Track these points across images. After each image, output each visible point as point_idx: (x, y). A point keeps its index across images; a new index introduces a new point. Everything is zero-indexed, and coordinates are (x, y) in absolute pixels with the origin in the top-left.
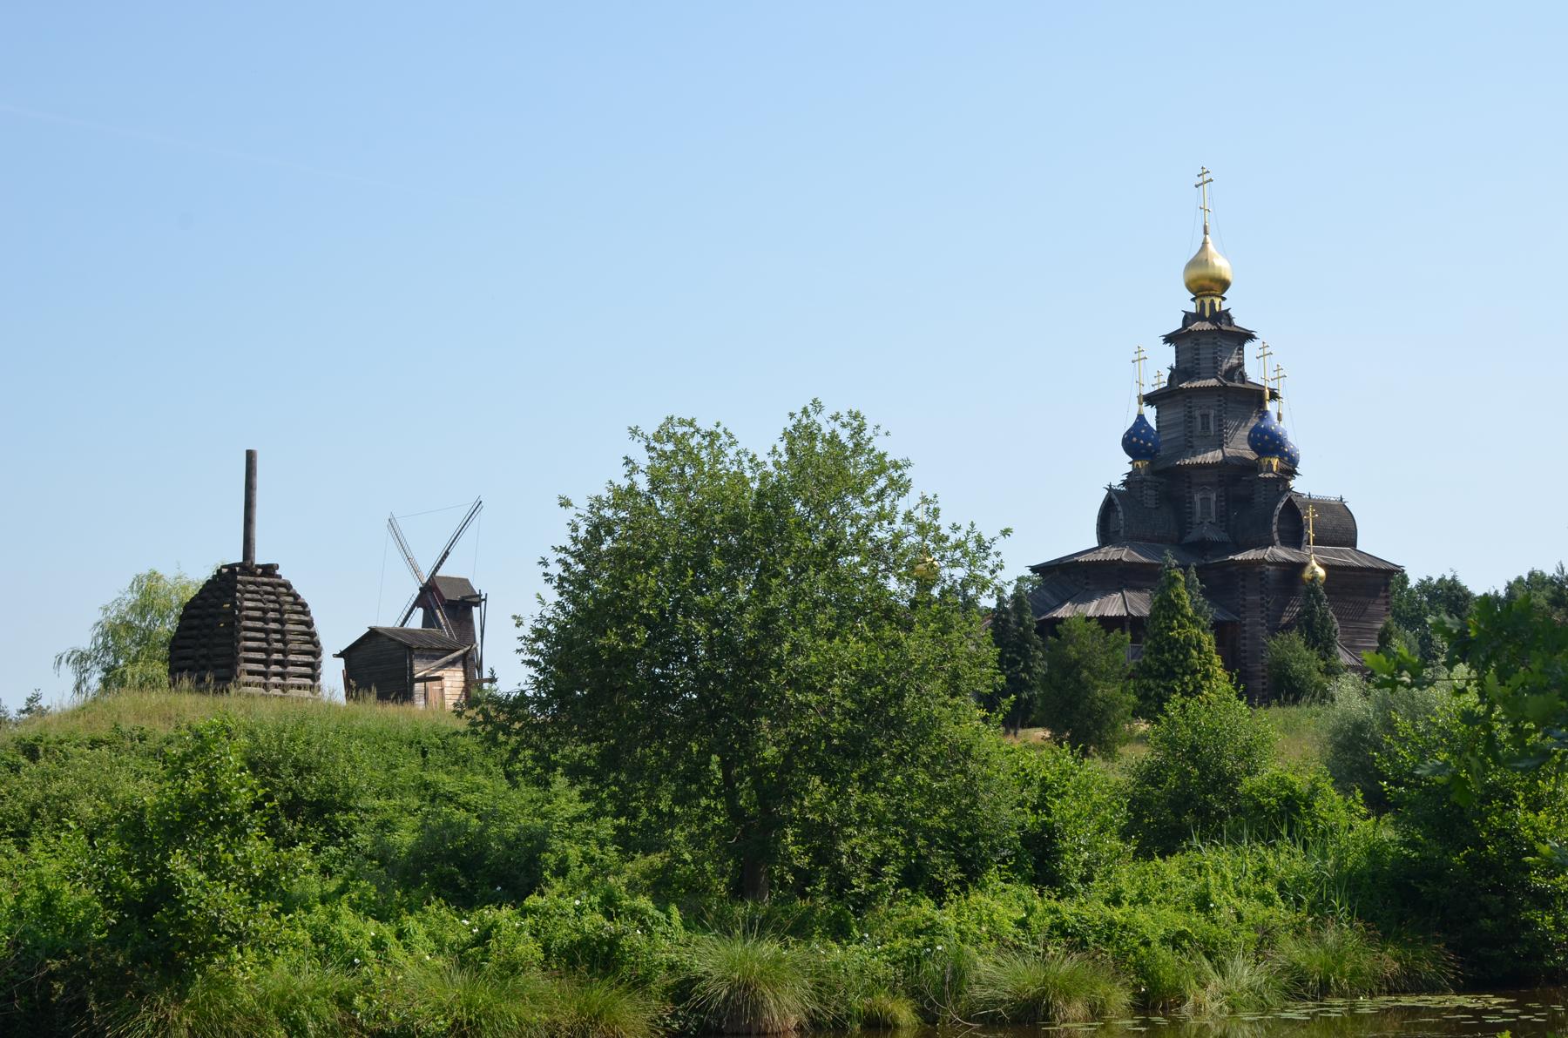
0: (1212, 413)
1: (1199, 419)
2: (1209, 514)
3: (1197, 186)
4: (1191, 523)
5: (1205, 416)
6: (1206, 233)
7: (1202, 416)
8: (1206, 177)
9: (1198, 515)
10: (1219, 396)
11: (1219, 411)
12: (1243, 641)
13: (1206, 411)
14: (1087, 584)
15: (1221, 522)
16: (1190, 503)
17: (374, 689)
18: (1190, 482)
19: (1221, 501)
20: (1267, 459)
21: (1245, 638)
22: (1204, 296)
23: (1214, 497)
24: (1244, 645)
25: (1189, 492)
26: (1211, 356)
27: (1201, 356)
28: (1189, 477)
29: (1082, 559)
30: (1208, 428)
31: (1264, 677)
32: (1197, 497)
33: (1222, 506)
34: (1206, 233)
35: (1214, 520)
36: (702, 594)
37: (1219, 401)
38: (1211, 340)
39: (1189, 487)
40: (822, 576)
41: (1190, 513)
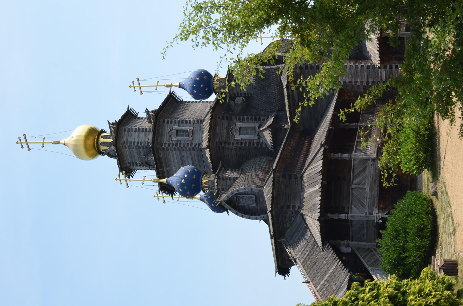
0: (176, 127)
1: (179, 138)
2: (252, 128)
3: (29, 149)
4: (258, 144)
5: (178, 133)
6: (58, 143)
7: (177, 136)
8: (23, 141)
9: (252, 137)
10: (164, 122)
11: (175, 123)
12: (359, 84)
13: (174, 132)
14: (294, 207)
15: (260, 119)
16: (242, 143)
17: (316, 73)
18: (225, 143)
19: (243, 119)
20: (215, 82)
21: (356, 82)
22: (97, 143)
23: (239, 124)
24: (362, 82)
25: (233, 144)
26: (137, 133)
27: (136, 141)
28: (221, 143)
29: (272, 233)
30: (187, 131)
31: (391, 67)
32: (238, 137)
33: (247, 118)
34: (58, 143)
35: (258, 125)
36: (370, 290)
37: (168, 122)
38: (126, 133)
39: (229, 144)
40: (418, 286)
41: (250, 143)
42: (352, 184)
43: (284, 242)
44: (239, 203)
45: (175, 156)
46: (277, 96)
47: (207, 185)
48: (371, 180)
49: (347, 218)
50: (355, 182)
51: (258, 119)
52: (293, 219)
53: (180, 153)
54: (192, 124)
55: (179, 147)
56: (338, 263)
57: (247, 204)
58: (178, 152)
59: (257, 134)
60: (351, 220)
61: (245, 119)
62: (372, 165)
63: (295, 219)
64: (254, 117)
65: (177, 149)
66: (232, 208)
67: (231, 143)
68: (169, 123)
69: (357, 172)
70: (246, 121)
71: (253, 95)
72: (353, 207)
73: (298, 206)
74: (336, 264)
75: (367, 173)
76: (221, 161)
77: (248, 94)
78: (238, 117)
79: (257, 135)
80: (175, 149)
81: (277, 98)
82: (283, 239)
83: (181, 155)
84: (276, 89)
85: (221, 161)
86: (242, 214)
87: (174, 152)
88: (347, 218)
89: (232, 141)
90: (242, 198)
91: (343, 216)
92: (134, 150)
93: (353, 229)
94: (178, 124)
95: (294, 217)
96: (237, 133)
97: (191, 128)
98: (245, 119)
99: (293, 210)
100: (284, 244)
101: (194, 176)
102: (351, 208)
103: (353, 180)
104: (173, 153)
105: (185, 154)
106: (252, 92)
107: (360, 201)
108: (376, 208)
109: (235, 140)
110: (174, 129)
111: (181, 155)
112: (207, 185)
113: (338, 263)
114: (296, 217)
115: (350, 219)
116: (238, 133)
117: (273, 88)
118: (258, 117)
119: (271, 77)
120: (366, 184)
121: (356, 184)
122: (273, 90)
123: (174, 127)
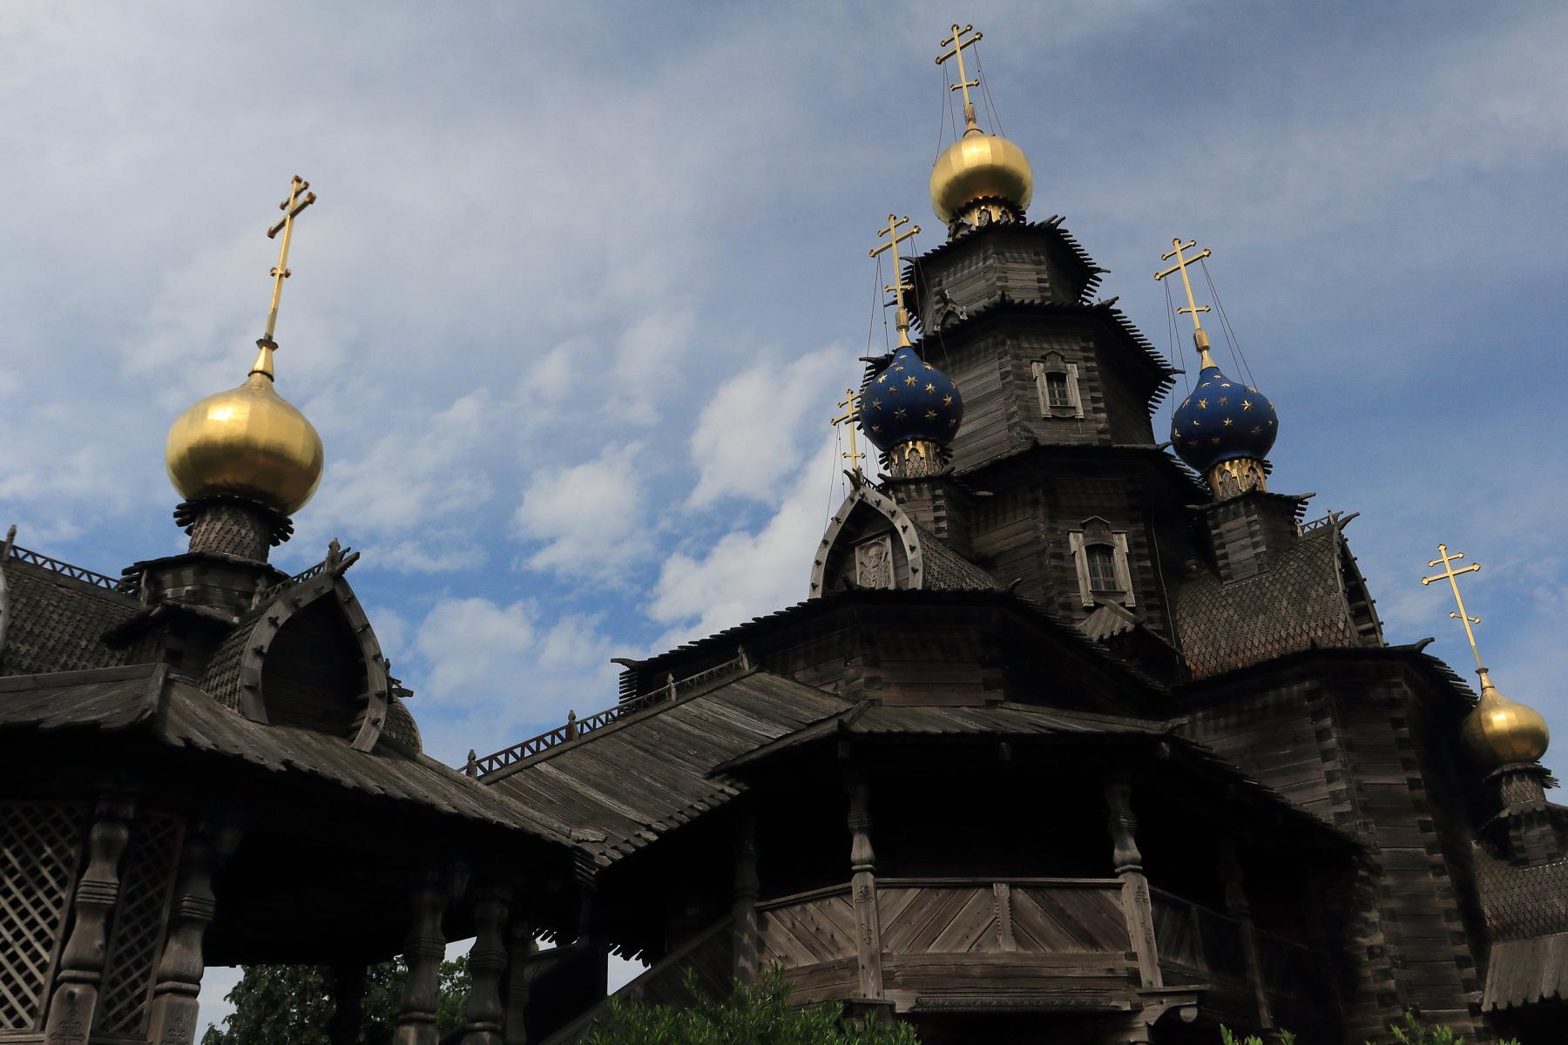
1: (1042, 384)
42: (1012, 886)
43: (737, 665)
44: (862, 548)
45: (985, 380)
46: (1241, 655)
47: (907, 458)
48: (1046, 972)
49: (854, 868)
50: (1021, 896)
51: (1149, 601)
52: (829, 689)
53: (998, 392)
54: (877, 1029)
55: (1016, 385)
56: (649, 828)
57: (862, 573)
58: (999, 385)
59: (1098, 601)
60: (848, 892)
61: (1142, 564)
62: (1111, 970)
63: (829, 694)
64: (1153, 588)
65: (1008, 380)
66: (841, 525)
67: (1054, 526)
68: (1085, 354)
69: (1070, 903)
70: (1136, 565)
71: (1225, 583)
72: (912, 894)
73: (881, 700)
74: (647, 820)
75: (1071, 950)
76: (991, 494)
77: (1227, 566)
78: (1144, 539)
79: (1095, 603)
80: (1004, 376)
81: (1234, 657)
82: (747, 666)
83: (989, 397)
84: (1269, 648)
85: (991, 494)
86: (824, 561)
87: (997, 375)
88: (854, 868)
89: (1061, 528)
90: (881, 553)
91: (861, 850)
92: (981, 284)
93: (811, 907)
94: (1086, 377)
95: (835, 689)
96: (1092, 539)
97: (1081, 414)
98: (1142, 564)
99: (862, 680)
100: (730, 665)
101: (932, 414)
102: (905, 887)
103: (1027, 887)
104: (991, 372)
105: (992, 406)
106: (1236, 578)
107: (940, 924)
108: (917, 1001)
109: (1068, 534)
110: (1069, 366)
111: (989, 397)
112: (907, 458)
113: (649, 828)
114: (837, 696)
115: (852, 883)
116: (1092, 541)
117: (1270, 639)
118: (1155, 601)
119: (1313, 624)
120: (1021, 951)
121: (1011, 900)
122: (1263, 640)
123: (1075, 365)
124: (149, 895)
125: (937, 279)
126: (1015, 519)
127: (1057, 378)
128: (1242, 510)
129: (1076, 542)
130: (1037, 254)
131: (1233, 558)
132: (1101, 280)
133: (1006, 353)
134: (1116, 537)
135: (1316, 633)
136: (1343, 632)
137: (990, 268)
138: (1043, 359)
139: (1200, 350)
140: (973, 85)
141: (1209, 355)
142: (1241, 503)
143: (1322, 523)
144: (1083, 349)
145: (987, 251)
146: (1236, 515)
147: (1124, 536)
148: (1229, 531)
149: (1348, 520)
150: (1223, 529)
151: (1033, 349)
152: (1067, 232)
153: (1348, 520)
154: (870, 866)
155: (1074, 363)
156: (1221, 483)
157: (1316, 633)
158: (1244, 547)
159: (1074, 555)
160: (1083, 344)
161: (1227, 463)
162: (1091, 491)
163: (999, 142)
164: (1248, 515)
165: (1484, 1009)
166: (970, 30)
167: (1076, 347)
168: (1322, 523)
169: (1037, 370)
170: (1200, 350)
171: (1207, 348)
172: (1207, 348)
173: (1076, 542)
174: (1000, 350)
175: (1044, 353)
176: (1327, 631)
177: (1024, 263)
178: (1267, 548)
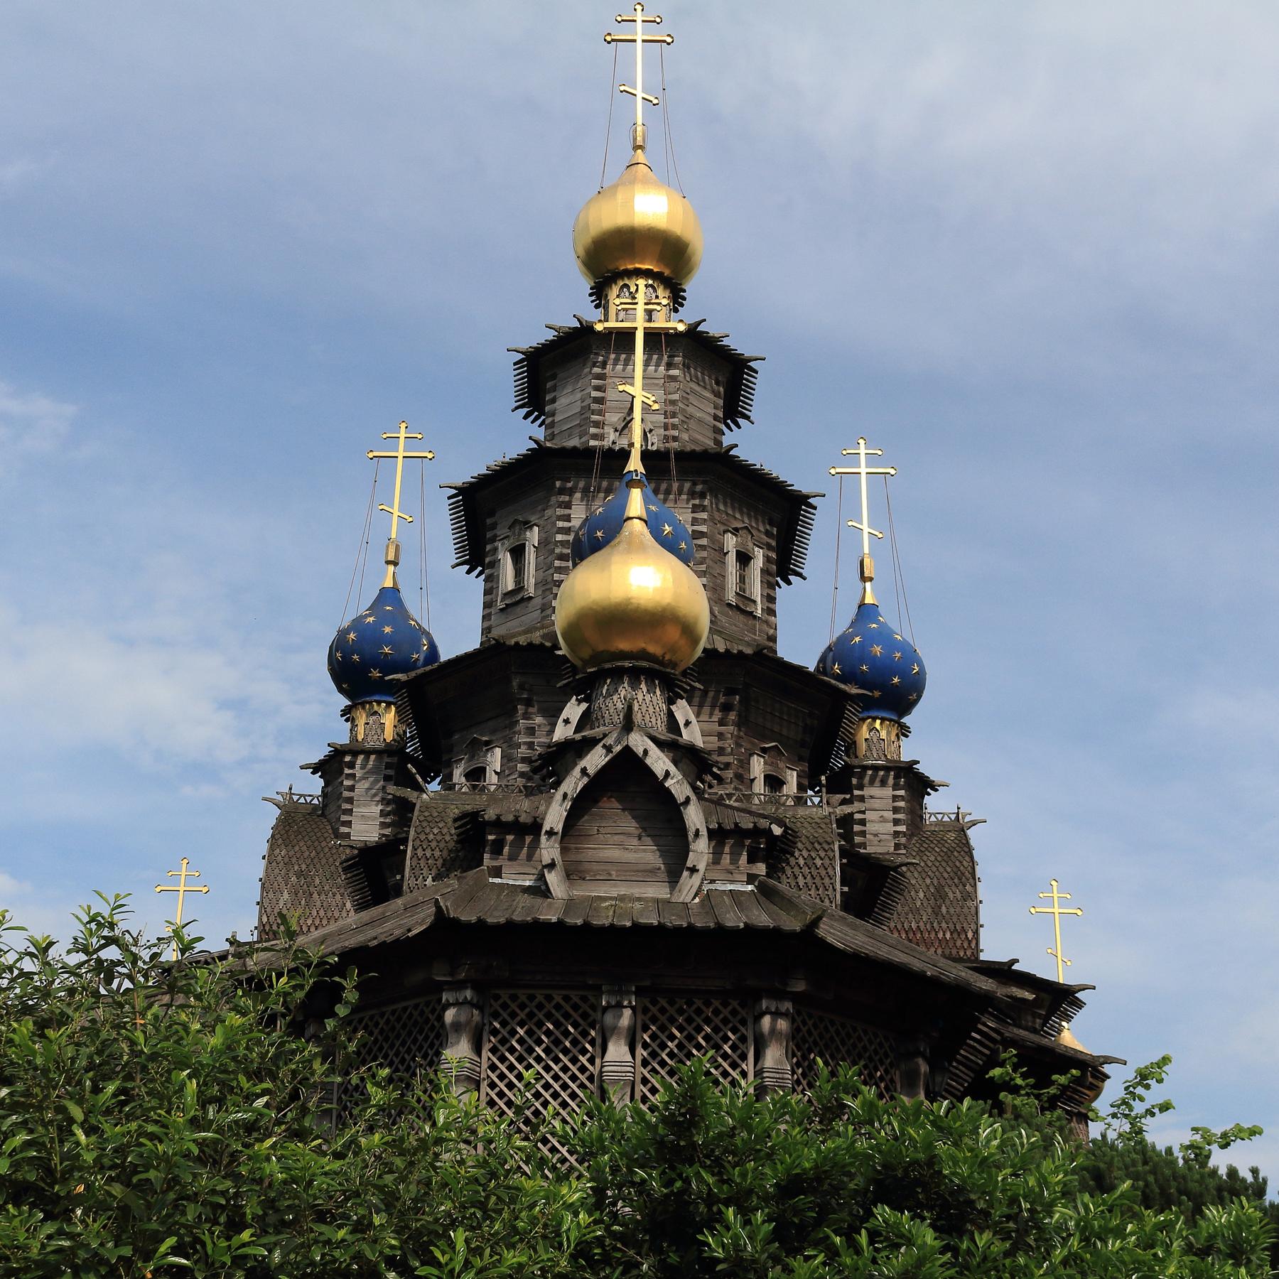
1: (731, 559)
110: (756, 549)
123: (761, 551)
124: (562, 1093)
125: (601, 359)
126: (710, 718)
127: (744, 559)
128: (891, 781)
129: (758, 767)
130: (717, 383)
131: (870, 827)
132: (739, 427)
133: (704, 509)
134: (789, 772)
135: (944, 935)
136: (970, 942)
137: (673, 379)
138: (735, 531)
139: (864, 579)
140: (651, 102)
141: (873, 589)
142: (892, 773)
143: (949, 818)
144: (768, 533)
145: (674, 356)
146: (883, 783)
147: (795, 773)
148: (872, 797)
149: (974, 823)
150: (867, 792)
151: (727, 514)
152: (757, 372)
153: (974, 823)
154: (1274, 1234)
155: (762, 548)
156: (866, 740)
157: (944, 935)
158: (883, 820)
159: (753, 780)
160: (768, 527)
161: (878, 722)
162: (777, 714)
163: (680, 205)
164: (896, 787)
165: (260, 1213)
166: (658, 23)
167: (762, 528)
168: (949, 818)
169: (731, 542)
170: (864, 579)
171: (871, 579)
172: (871, 579)
173: (758, 767)
174: (697, 502)
175: (739, 525)
176: (955, 936)
177: (705, 388)
178: (907, 829)
